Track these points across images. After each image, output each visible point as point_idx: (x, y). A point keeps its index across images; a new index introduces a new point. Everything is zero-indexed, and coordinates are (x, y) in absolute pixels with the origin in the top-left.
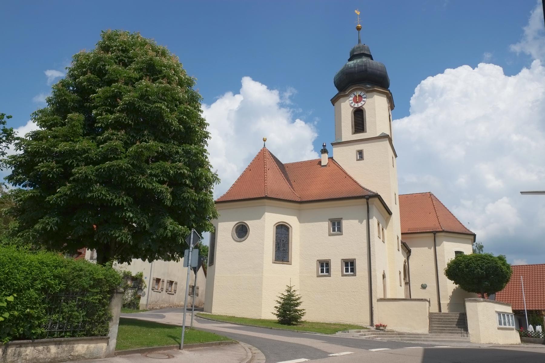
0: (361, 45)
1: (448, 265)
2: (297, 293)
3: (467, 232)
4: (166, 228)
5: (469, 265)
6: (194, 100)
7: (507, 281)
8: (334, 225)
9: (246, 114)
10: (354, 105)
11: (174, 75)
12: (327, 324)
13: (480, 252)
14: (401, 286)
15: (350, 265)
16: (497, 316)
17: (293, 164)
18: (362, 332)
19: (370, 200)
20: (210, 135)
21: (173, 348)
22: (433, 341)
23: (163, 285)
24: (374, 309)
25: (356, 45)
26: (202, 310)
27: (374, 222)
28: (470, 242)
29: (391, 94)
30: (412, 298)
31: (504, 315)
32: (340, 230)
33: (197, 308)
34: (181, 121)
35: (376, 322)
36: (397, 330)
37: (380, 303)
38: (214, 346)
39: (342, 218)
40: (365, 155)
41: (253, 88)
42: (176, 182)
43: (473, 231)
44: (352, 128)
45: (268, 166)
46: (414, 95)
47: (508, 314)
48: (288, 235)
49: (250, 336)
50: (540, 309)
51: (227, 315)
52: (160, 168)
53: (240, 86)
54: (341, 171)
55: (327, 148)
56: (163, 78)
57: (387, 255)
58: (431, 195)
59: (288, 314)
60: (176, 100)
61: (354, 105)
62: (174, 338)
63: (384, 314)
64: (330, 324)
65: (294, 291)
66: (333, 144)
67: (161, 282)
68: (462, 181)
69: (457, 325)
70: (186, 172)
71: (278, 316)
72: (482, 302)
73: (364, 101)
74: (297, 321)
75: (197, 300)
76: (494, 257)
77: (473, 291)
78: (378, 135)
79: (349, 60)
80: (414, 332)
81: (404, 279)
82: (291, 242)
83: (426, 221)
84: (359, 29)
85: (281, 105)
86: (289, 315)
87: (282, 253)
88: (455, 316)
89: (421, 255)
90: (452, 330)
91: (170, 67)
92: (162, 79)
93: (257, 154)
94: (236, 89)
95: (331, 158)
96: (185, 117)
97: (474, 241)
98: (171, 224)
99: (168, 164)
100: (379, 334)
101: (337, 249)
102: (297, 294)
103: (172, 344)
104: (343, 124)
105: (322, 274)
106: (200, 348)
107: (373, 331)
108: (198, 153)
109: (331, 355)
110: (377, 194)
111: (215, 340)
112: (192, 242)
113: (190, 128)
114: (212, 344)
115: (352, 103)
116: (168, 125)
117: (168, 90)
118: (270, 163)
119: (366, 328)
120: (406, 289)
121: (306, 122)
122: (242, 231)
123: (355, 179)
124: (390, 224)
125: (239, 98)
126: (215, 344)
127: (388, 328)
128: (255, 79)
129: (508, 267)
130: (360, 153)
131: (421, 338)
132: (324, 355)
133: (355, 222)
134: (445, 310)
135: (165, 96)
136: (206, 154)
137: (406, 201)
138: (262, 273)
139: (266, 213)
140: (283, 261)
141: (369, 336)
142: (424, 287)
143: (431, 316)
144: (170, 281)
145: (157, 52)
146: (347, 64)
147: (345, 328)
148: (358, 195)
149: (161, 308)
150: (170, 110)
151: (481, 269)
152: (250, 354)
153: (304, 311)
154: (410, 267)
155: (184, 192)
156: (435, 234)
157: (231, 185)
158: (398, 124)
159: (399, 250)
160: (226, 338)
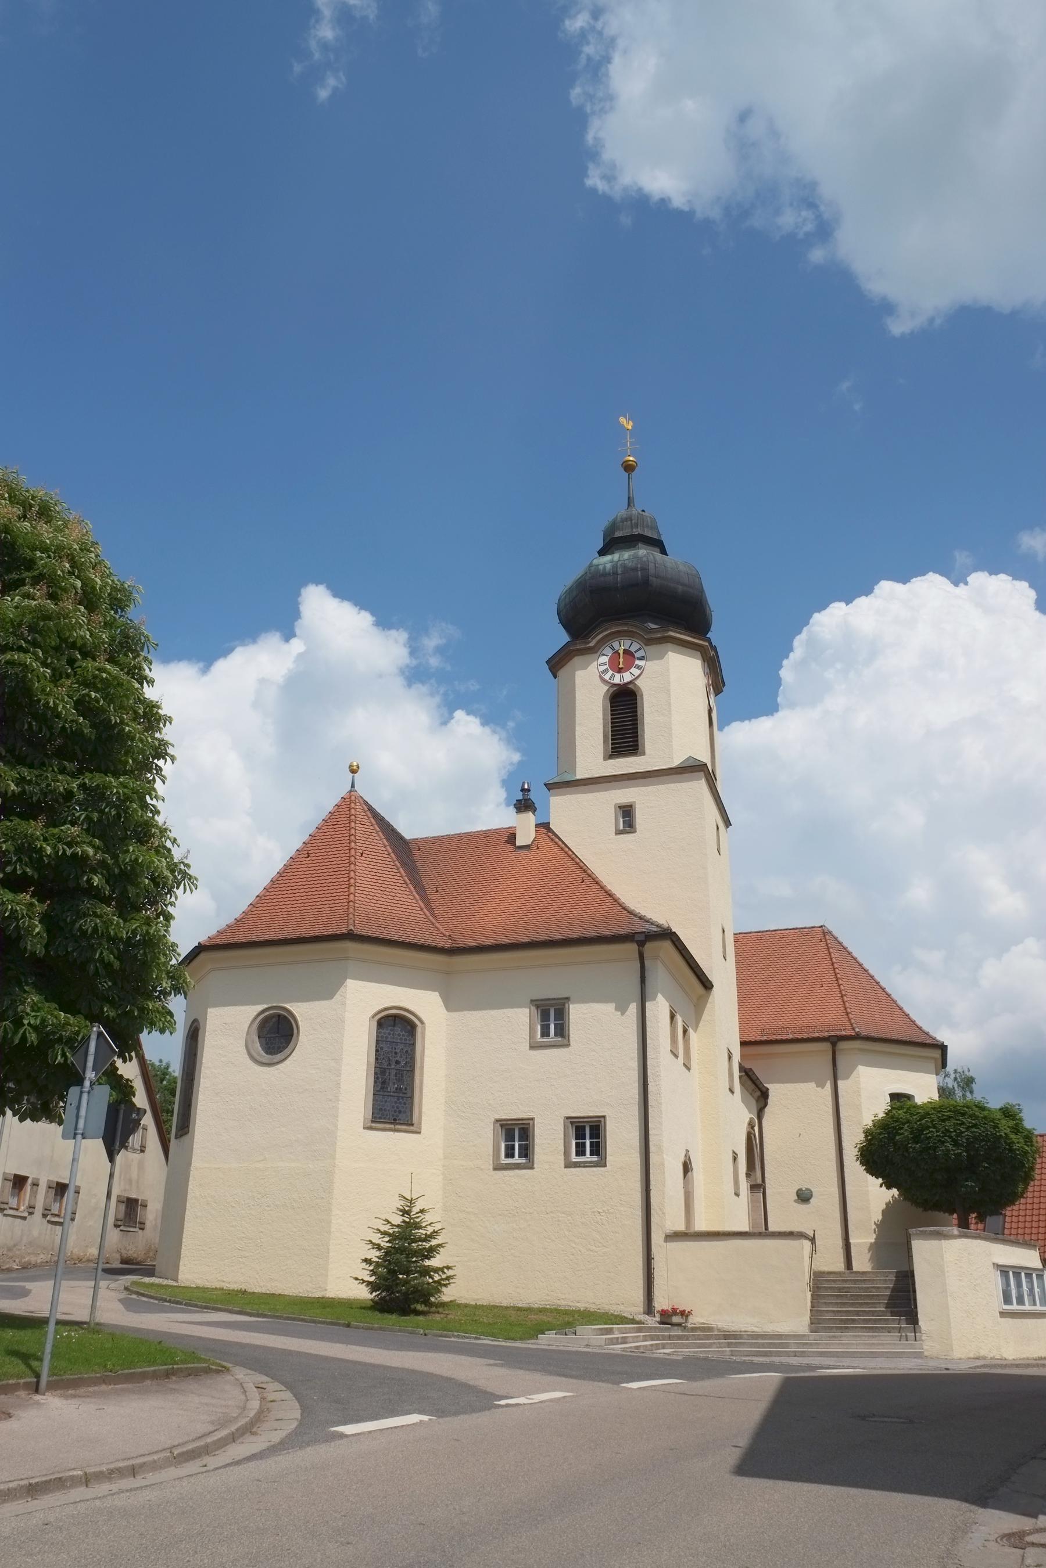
0: (635, 511)
1: (867, 1133)
2: (428, 1218)
4: (18, 1022)
5: (921, 1130)
6: (128, 650)
7: (1027, 1178)
8: (545, 1016)
9: (310, 696)
10: (613, 676)
11: (71, 573)
12: (520, 1309)
13: (964, 1096)
14: (737, 1194)
15: (588, 1135)
17: (435, 841)
18: (618, 1331)
19: (649, 946)
20: (170, 750)
21: (15, 1387)
22: (822, 1354)
23: (34, 1194)
25: (622, 511)
26: (150, 1272)
27: (659, 1008)
28: (932, 1066)
29: (715, 649)
30: (771, 1228)
31: (1017, 1275)
32: (562, 1031)
33: (129, 1266)
34: (82, 706)
35: (661, 1303)
36: (720, 1325)
37: (673, 1245)
38: (148, 1382)
41: (333, 622)
42: (58, 884)
43: (942, 1036)
44: (605, 741)
45: (360, 845)
46: (791, 655)
47: (1029, 1272)
48: (414, 1044)
49: (290, 1353)
51: (225, 1286)
52: (13, 839)
53: (295, 614)
54: (569, 862)
55: (532, 796)
56: (36, 581)
57: (698, 1105)
58: (825, 933)
59: (405, 1281)
60: (73, 646)
61: (613, 676)
62: (25, 1357)
63: (690, 1281)
64: (529, 1310)
65: (422, 1211)
66: (549, 786)
67: (28, 1187)
68: (920, 893)
69: (887, 1306)
70: (91, 851)
71: (373, 1287)
73: (639, 667)
74: (427, 1302)
75: (137, 1244)
76: (989, 1110)
77: (937, 1207)
78: (676, 763)
79: (602, 552)
80: (770, 1328)
81: (748, 1175)
82: (422, 1068)
83: (811, 1008)
84: (629, 468)
85: (415, 675)
86: (406, 1282)
87: (393, 1097)
88: (885, 1284)
89: (798, 1106)
90: (875, 1321)
91: (60, 551)
92: (33, 585)
93: (330, 808)
94: (285, 621)
96: (93, 694)
97: (944, 1065)
98: (35, 1008)
99: (35, 828)
100: (670, 1337)
101: (553, 1088)
102: (432, 1220)
103: (12, 1377)
104: (579, 730)
105: (510, 1161)
106: (104, 1387)
107: (650, 1329)
108: (128, 798)
109: (503, 1402)
110: (669, 929)
111: (153, 1363)
112: (90, 1064)
113: (109, 726)
114: (144, 1376)
115: (605, 671)
116: (47, 717)
117: (49, 618)
118: (367, 836)
119: (633, 1321)
120: (752, 1203)
121: (486, 721)
122: (276, 1034)
123: (609, 887)
125: (297, 646)
126: (155, 1376)
127: (695, 1320)
128: (339, 592)
129: (1029, 1137)
130: (627, 812)
131: (787, 1345)
132: (483, 1400)
134: (862, 1263)
135: (39, 632)
136: (154, 802)
137: (754, 950)
140: (395, 1121)
141: (636, 1342)
142: (804, 1197)
143: (819, 1282)
144: (58, 1184)
145: (26, 506)
146: (595, 562)
147: (567, 1320)
148: (615, 932)
149: (25, 1267)
150: (53, 675)
151: (956, 1144)
152: (255, 1405)
153: (449, 1273)
155: (85, 915)
156: (834, 1045)
157: (251, 899)
158: (743, 736)
159: (732, 1091)
160: (193, 1357)
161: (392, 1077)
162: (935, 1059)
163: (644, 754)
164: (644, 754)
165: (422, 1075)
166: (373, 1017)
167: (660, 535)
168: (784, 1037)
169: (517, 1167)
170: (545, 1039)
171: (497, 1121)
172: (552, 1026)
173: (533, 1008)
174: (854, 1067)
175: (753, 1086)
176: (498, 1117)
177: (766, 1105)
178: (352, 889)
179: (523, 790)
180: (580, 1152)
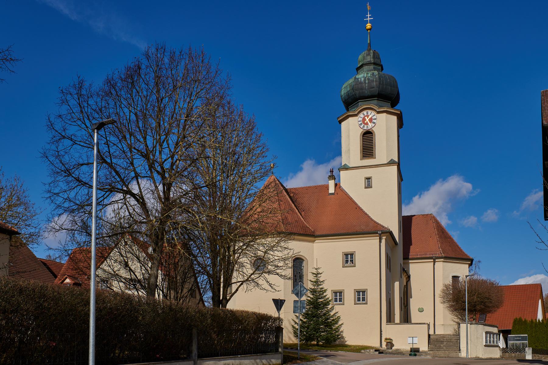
10: (364, 127)
24: (383, 333)
40: (374, 182)
61: (364, 127)
115: (361, 124)
169: (339, 304)
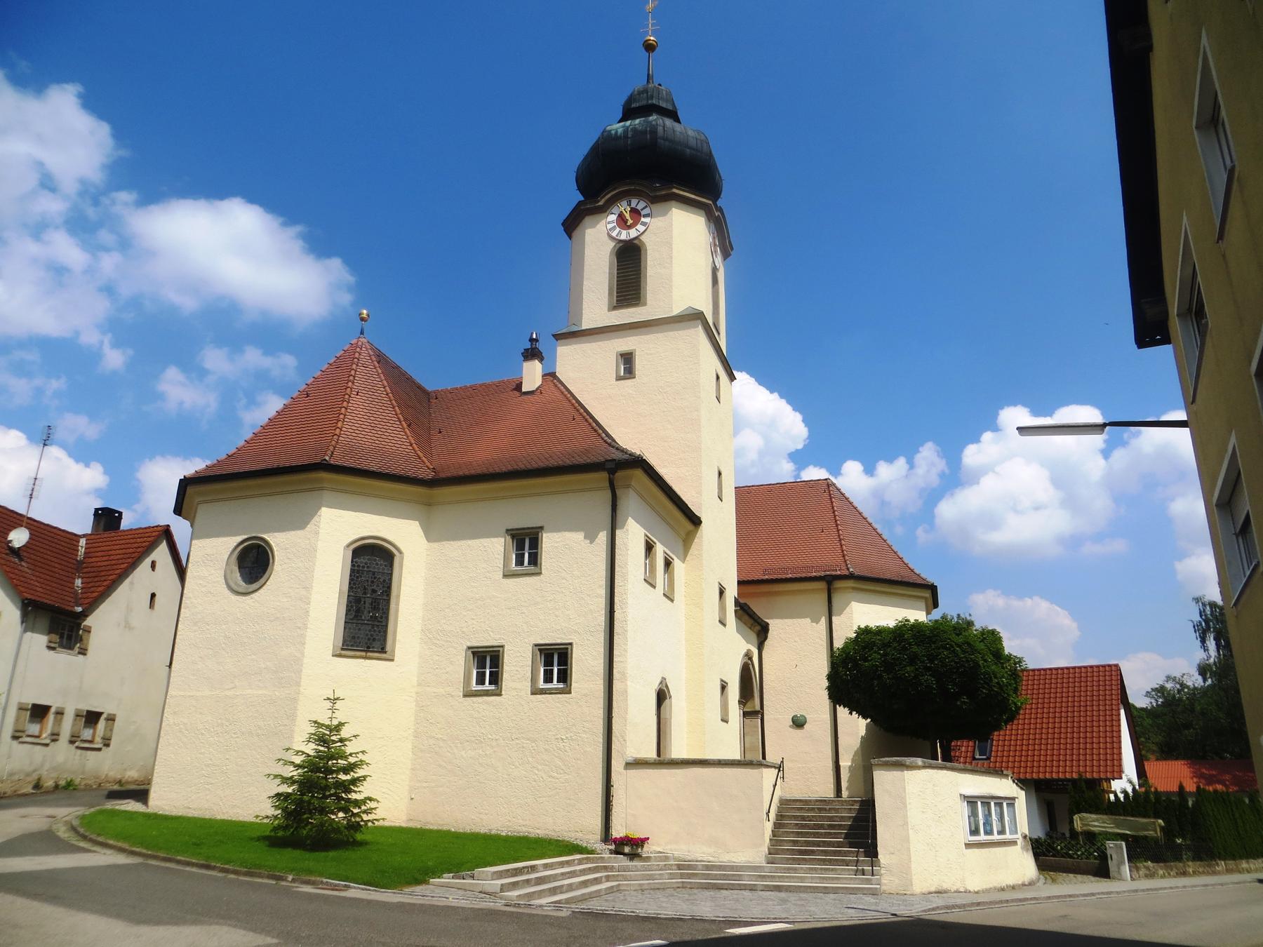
3: (913, 579)
8: (520, 547)
10: (620, 233)
15: (555, 661)
16: (965, 809)
19: (619, 474)
24: (614, 791)
25: (640, 83)
27: (633, 535)
28: (923, 605)
39: (541, 528)
43: (931, 578)
50: (1095, 776)
59: (318, 813)
61: (620, 233)
63: (642, 806)
67: (51, 717)
69: (847, 836)
72: (919, 768)
73: (644, 224)
80: (726, 858)
82: (398, 596)
84: (649, 48)
88: (847, 815)
95: (550, 376)
101: (521, 615)
105: (480, 688)
115: (614, 228)
122: (254, 563)
124: (694, 550)
133: (575, 538)
138: (298, 684)
139: (324, 509)
140: (368, 649)
154: (764, 670)
159: (723, 623)
161: (367, 605)
162: (926, 599)
163: (645, 304)
164: (645, 304)
165: (397, 604)
166: (348, 546)
167: (673, 104)
168: (784, 576)
169: (487, 693)
170: (519, 568)
171: (469, 648)
172: (527, 556)
173: (509, 538)
174: (848, 604)
175: (751, 621)
176: (469, 644)
177: (766, 638)
178: (340, 425)
179: (531, 340)
180: (548, 679)
